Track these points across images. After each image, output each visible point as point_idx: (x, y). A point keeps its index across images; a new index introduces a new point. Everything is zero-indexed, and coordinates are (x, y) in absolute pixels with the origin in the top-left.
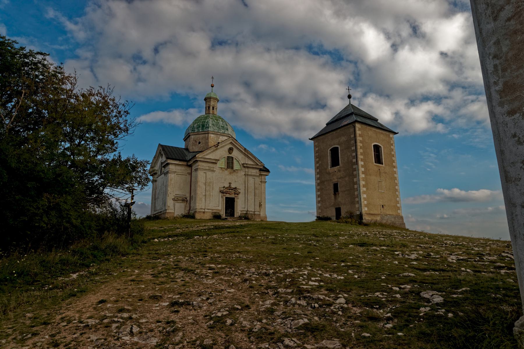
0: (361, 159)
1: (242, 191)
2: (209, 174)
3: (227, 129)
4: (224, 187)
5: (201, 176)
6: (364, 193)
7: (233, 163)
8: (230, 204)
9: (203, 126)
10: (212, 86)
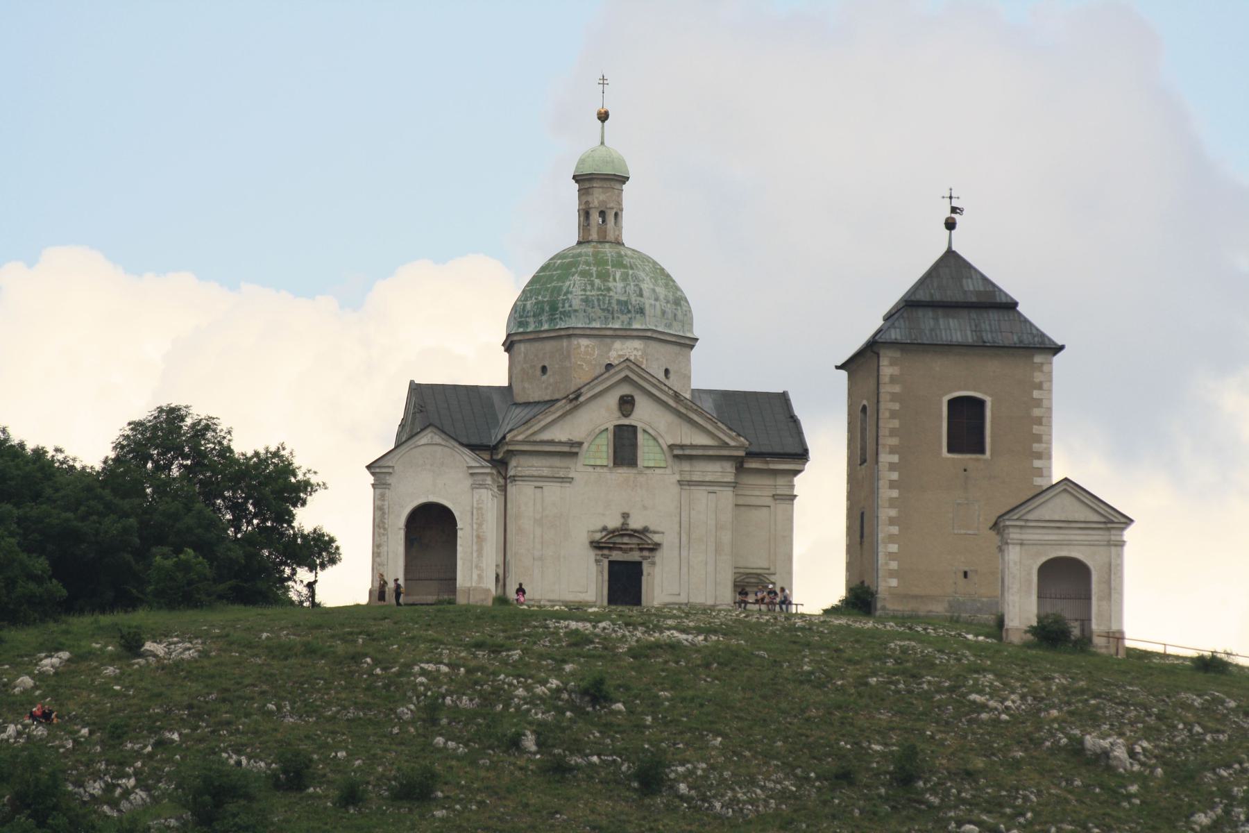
0: (891, 482)
1: (668, 539)
2: (553, 491)
3: (641, 311)
4: (605, 529)
6: (891, 538)
7: (634, 446)
8: (625, 582)
9: (554, 308)
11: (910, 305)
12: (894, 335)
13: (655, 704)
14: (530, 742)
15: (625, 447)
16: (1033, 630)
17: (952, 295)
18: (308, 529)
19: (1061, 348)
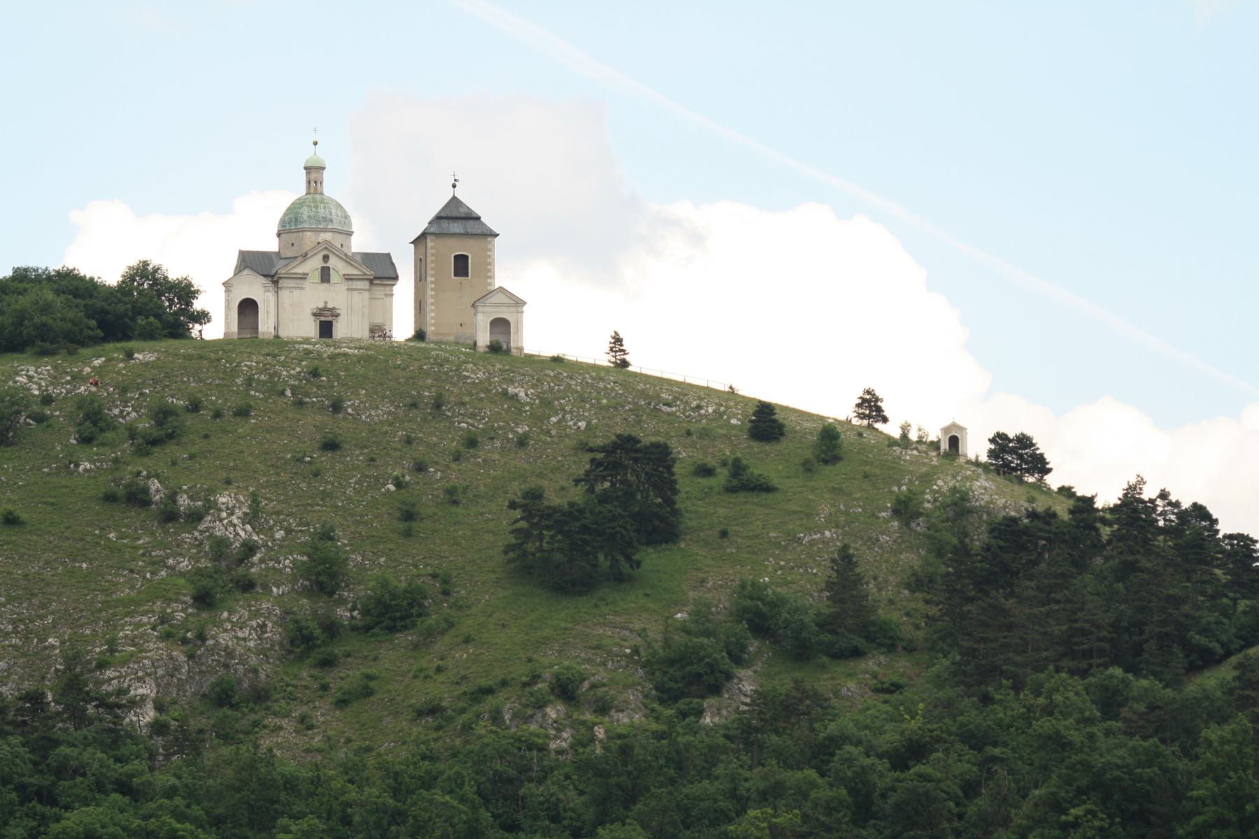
1: (343, 312)
6: (432, 311)
8: (326, 329)
10: (315, 144)
11: (439, 218)
12: (432, 230)
13: (339, 377)
14: (288, 393)
15: (325, 275)
18: (199, 309)
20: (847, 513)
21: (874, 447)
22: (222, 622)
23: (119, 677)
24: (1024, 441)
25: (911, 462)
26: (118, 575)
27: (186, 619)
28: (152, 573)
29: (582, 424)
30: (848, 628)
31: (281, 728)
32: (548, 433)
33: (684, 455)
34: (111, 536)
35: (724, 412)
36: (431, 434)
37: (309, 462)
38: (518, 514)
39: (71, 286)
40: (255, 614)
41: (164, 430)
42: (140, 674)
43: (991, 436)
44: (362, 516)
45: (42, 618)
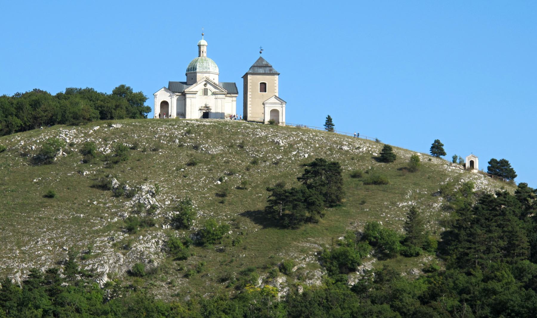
5: (188, 101)
7: (207, 92)
11: (253, 67)
12: (250, 72)
13: (200, 135)
14: (177, 141)
15: (205, 92)
16: (269, 122)
17: (261, 65)
18: (146, 106)
19: (329, 116)
20: (420, 193)
21: (436, 165)
22: (140, 240)
23: (93, 264)
24: (504, 163)
25: (451, 172)
26: (95, 220)
27: (124, 239)
28: (111, 219)
29: (306, 155)
30: (410, 244)
31: (162, 286)
32: (290, 159)
33: (348, 168)
34: (94, 203)
35: (371, 150)
36: (238, 159)
37: (183, 172)
38: (271, 193)
39: (88, 95)
40: (155, 237)
41: (120, 156)
42: (102, 262)
43: (489, 161)
44: (204, 194)
45: (63, 237)
